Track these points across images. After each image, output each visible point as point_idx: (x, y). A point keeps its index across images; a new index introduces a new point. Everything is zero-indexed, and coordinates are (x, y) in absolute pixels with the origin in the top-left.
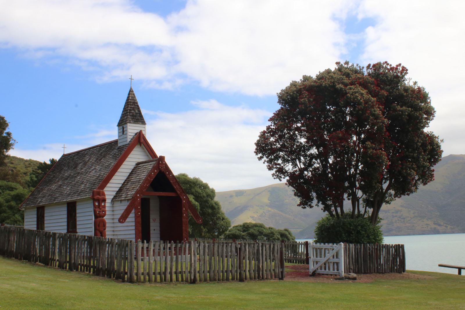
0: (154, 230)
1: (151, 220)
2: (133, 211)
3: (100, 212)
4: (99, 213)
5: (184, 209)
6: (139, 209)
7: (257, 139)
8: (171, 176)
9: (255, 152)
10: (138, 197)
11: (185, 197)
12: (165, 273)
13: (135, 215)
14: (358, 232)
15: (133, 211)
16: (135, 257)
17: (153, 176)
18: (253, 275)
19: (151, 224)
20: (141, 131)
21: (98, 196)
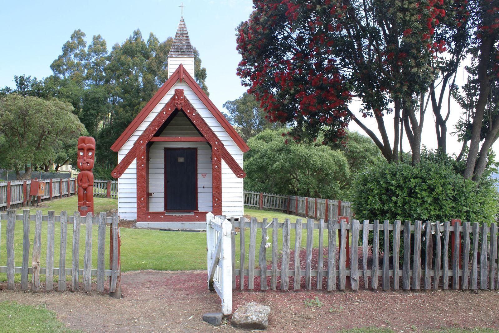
0: (204, 187)
1: (199, 176)
2: (135, 161)
3: (83, 164)
4: (82, 165)
5: (215, 159)
6: (143, 159)
7: (237, 24)
8: (194, 114)
9: (99, 37)
10: (142, 144)
11: (216, 143)
12: (327, 253)
13: (137, 166)
14: (412, 193)
15: (135, 161)
16: (371, 229)
17: (164, 115)
18: (484, 279)
19: (199, 181)
20: (181, 66)
21: (83, 144)
